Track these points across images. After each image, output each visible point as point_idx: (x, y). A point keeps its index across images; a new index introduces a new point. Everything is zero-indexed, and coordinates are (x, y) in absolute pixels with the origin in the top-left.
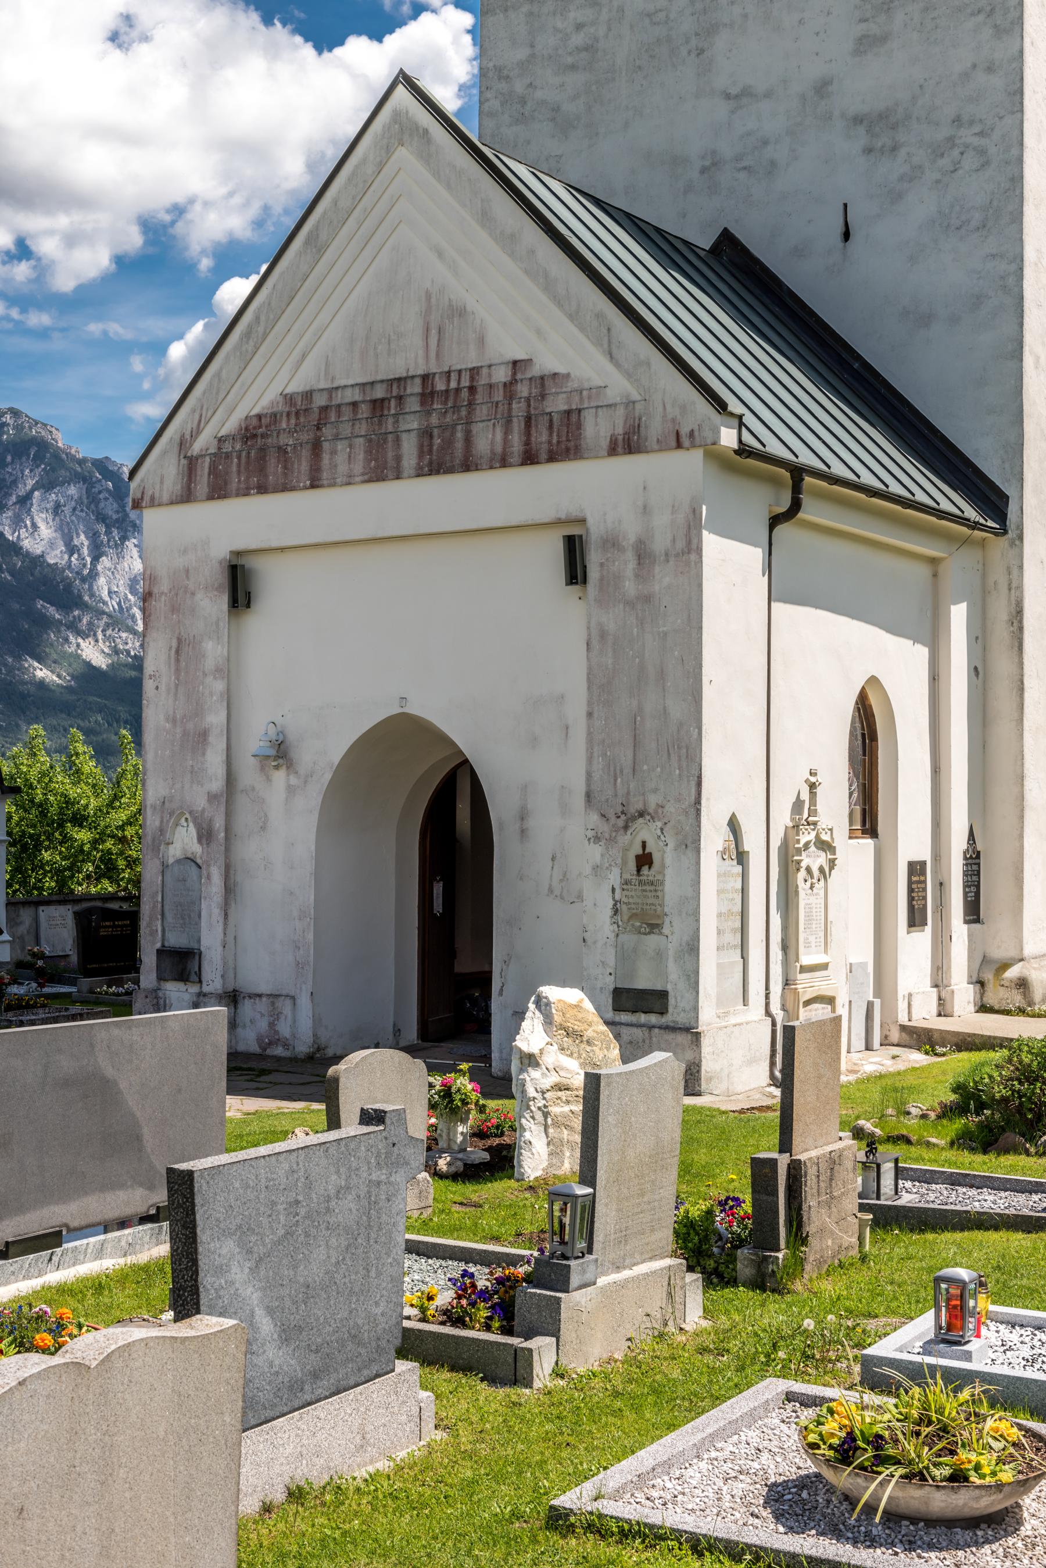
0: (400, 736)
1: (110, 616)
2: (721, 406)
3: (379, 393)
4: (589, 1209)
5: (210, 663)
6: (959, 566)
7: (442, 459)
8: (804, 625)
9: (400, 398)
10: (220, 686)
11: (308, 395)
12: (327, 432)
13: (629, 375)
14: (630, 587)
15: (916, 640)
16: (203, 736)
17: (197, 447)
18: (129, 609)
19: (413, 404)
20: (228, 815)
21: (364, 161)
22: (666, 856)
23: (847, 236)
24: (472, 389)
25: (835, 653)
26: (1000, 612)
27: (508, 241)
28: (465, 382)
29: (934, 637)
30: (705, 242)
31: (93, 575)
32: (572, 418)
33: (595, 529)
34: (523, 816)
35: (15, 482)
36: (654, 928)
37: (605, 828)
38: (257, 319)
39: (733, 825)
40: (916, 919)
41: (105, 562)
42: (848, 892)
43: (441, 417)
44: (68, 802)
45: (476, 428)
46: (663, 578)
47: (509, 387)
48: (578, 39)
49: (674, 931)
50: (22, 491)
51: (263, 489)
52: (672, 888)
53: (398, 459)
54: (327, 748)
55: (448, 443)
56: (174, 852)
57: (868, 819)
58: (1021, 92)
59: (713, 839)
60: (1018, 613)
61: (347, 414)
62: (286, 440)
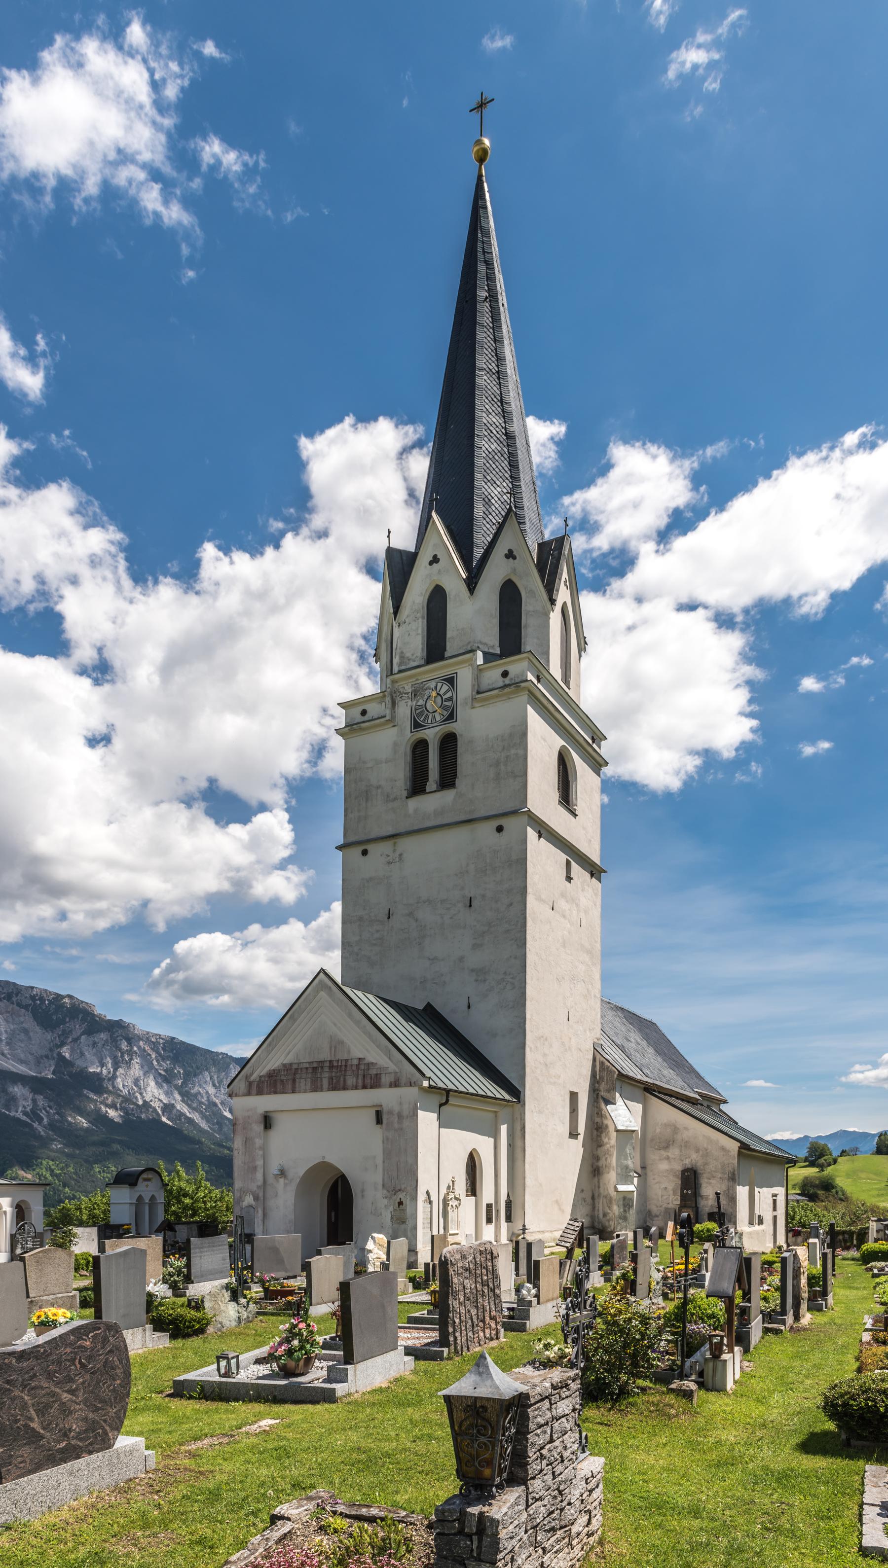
0: (323, 1167)
1: (123, 1097)
2: (423, 1075)
3: (315, 1065)
4: (388, 1265)
5: (257, 1145)
6: (504, 1113)
7: (334, 1087)
8: (451, 1135)
9: (322, 1067)
10: (261, 1153)
11: (291, 1064)
12: (298, 1076)
13: (395, 1065)
14: (396, 1125)
15: (489, 1136)
16: (255, 1168)
17: (252, 1078)
18: (134, 1094)
19: (326, 1069)
20: (264, 1192)
21: (309, 994)
22: (407, 1202)
23: (469, 1007)
24: (346, 1066)
25: (461, 1142)
26: (518, 1127)
27: (357, 1023)
28: (344, 1063)
29: (495, 1135)
30: (421, 1007)
31: (114, 1077)
32: (378, 1076)
33: (385, 1109)
34: (363, 1191)
35: (71, 1031)
36: (404, 1223)
37: (388, 1194)
38: (273, 1040)
39: (428, 1193)
40: (489, 1221)
41: (121, 1071)
42: (465, 1214)
43: (334, 1073)
44: (181, 1189)
45: (347, 1078)
46: (406, 1123)
47: (358, 1066)
48: (376, 935)
49: (409, 1224)
50: (75, 1035)
51: (275, 1093)
52: (409, 1211)
53: (322, 1086)
54: (299, 1171)
55: (338, 1082)
56: (245, 1204)
57: (473, 1189)
58: (525, 966)
59: (421, 1197)
60: (523, 1128)
61: (304, 1071)
62: (283, 1078)
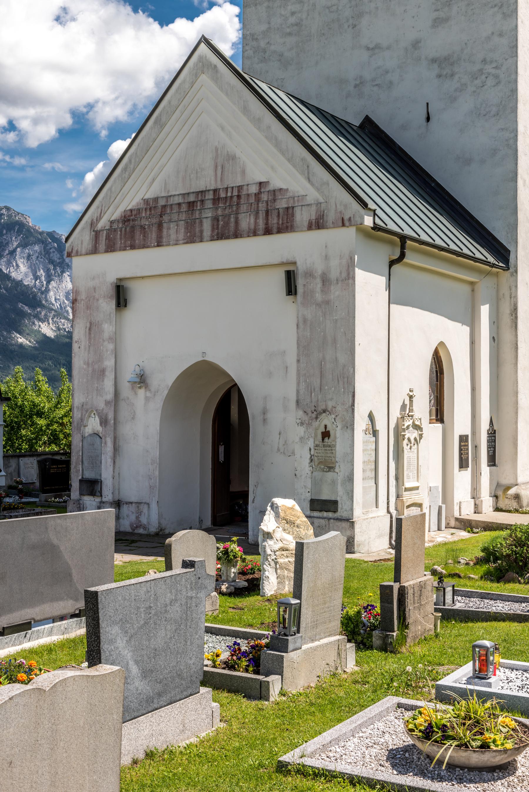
0: (202, 372)
1: (55, 311)
2: (365, 205)
3: (192, 198)
4: (298, 611)
5: (106, 335)
6: (485, 286)
7: (223, 232)
8: (407, 316)
9: (202, 201)
10: (111, 346)
11: (156, 200)
12: (166, 218)
13: (318, 190)
14: (319, 297)
15: (463, 323)
16: (103, 372)
17: (100, 226)
18: (65, 308)
19: (209, 204)
20: (116, 412)
21: (184, 81)
22: (337, 432)
23: (428, 119)
24: (239, 197)
25: (422, 330)
26: (506, 309)
27: (257, 122)
28: (235, 193)
29: (472, 322)
30: (357, 122)
31: (47, 290)
32: (289, 211)
33: (301, 267)
34: (264, 412)
35: (7, 244)
36: (331, 469)
37: (306, 418)
38: (130, 161)
39: (371, 417)
40: (463, 464)
41: (53, 284)
42: (429, 451)
43: (223, 210)
44: (35, 405)
45: (241, 216)
46: (335, 292)
47: (258, 195)
48: (292, 20)
49: (341, 470)
50: (11, 248)
51: (133, 247)
52: (340, 449)
53: (201, 232)
54: (165, 378)
55: (227, 224)
56: (88, 430)
57: (439, 414)
58: (516, 46)
59: (361, 424)
60: (515, 310)
61: (175, 209)
62: (144, 222)
